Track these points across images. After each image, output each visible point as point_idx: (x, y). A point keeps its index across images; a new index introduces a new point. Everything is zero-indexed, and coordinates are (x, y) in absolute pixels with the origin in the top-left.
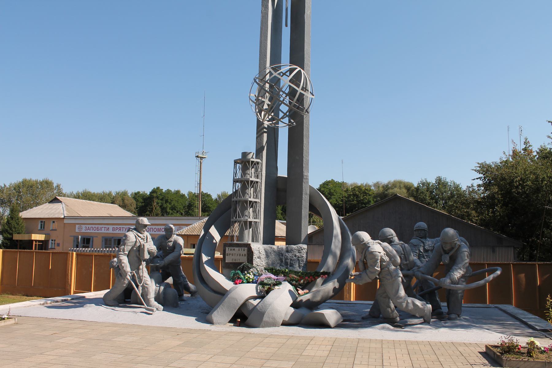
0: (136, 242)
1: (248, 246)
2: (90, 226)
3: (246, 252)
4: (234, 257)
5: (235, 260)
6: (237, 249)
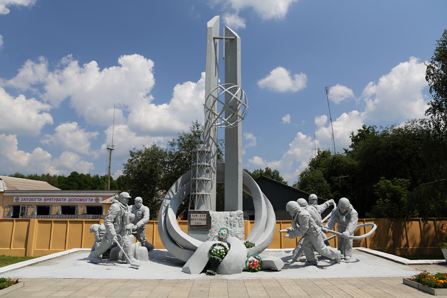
0: (121, 211)
1: (207, 213)
2: (26, 198)
3: (205, 218)
4: (197, 221)
5: (198, 223)
6: (199, 215)
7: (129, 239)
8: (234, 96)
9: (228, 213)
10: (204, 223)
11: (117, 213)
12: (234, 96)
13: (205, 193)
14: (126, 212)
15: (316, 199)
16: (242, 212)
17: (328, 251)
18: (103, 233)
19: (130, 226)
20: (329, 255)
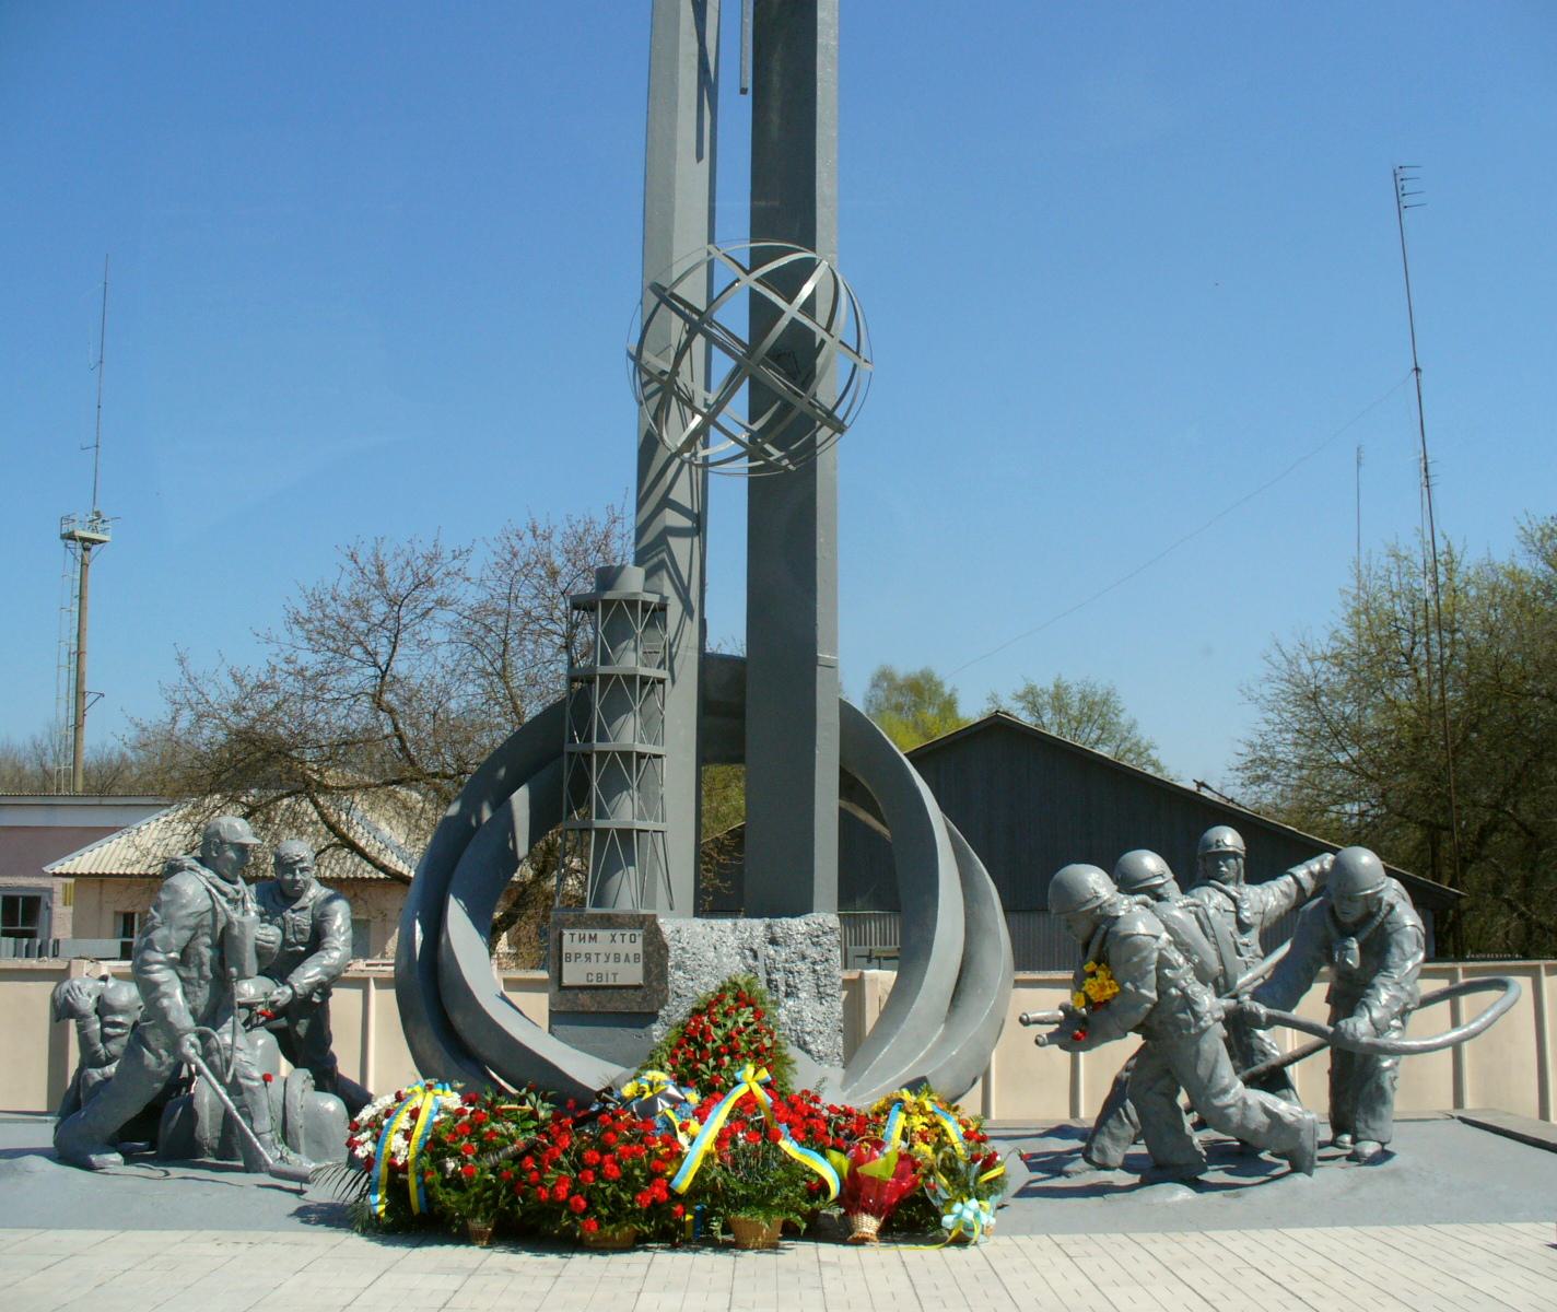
0: (213, 910)
3: (638, 947)
4: (596, 967)
5: (599, 976)
7: (255, 1051)
8: (791, 311)
9: (758, 926)
10: (633, 974)
11: (192, 922)
12: (791, 311)
13: (643, 671)
14: (236, 916)
15: (1235, 855)
16: (833, 920)
17: (1251, 1114)
18: (119, 1025)
19: (251, 989)
20: (1256, 1132)
